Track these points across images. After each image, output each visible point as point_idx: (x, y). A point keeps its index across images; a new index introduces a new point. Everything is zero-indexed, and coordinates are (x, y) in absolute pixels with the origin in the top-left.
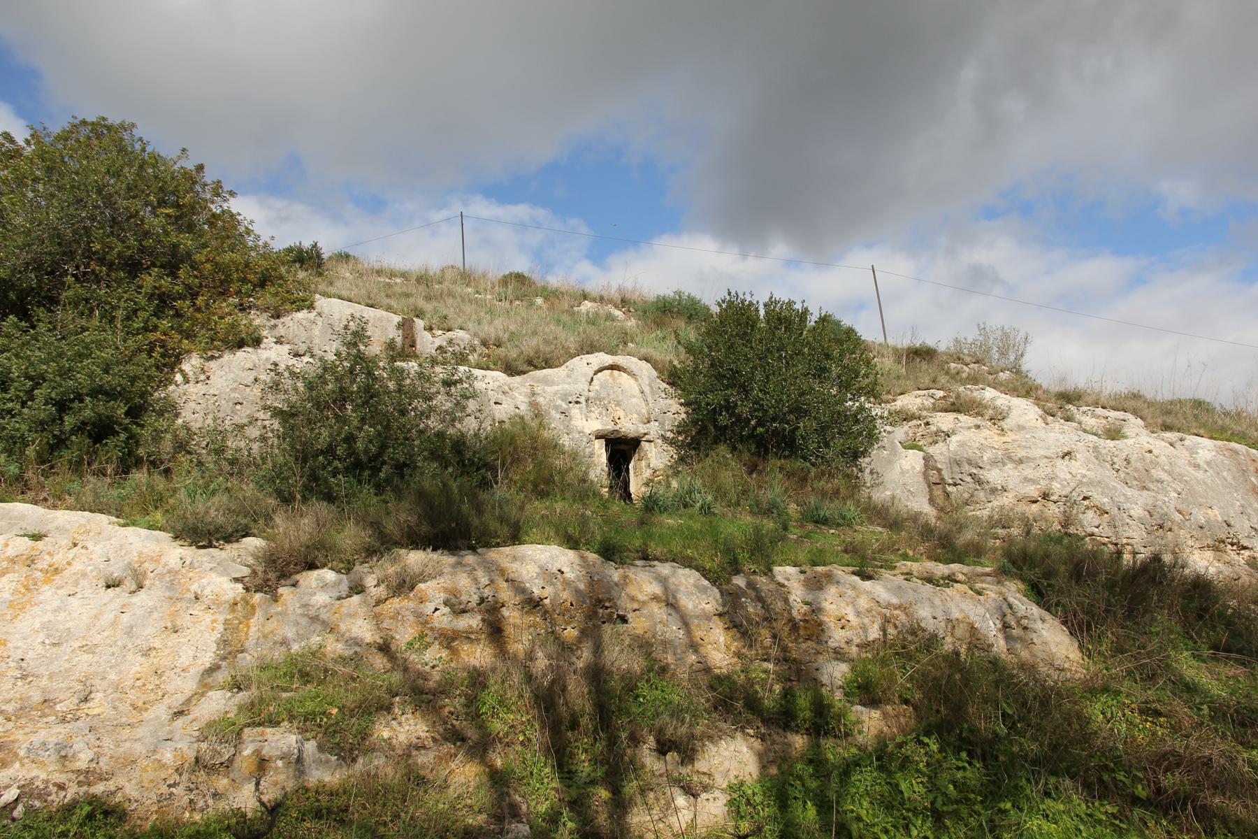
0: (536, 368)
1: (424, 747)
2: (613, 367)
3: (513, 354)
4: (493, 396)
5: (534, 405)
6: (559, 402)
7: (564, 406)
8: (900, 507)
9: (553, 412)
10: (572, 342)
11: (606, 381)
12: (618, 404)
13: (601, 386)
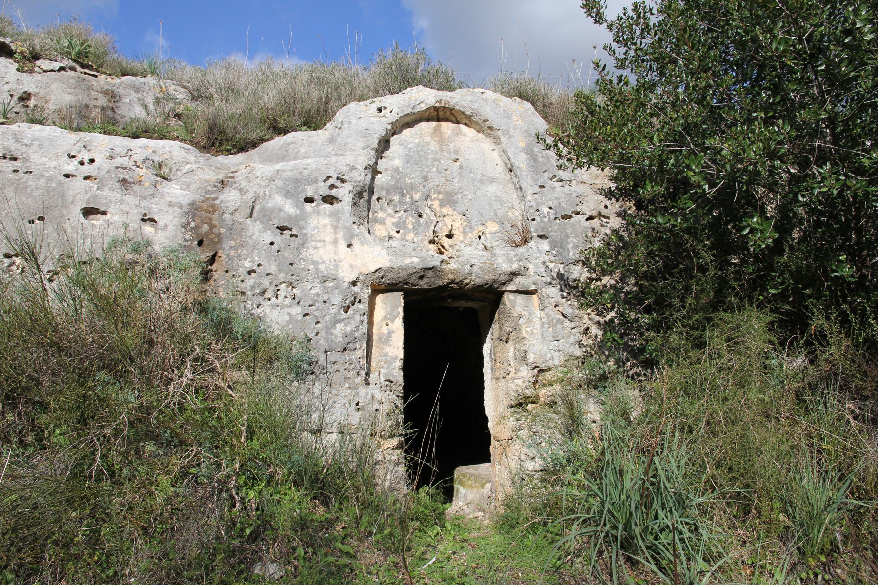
2: (439, 114)
7: (290, 208)
12: (449, 200)
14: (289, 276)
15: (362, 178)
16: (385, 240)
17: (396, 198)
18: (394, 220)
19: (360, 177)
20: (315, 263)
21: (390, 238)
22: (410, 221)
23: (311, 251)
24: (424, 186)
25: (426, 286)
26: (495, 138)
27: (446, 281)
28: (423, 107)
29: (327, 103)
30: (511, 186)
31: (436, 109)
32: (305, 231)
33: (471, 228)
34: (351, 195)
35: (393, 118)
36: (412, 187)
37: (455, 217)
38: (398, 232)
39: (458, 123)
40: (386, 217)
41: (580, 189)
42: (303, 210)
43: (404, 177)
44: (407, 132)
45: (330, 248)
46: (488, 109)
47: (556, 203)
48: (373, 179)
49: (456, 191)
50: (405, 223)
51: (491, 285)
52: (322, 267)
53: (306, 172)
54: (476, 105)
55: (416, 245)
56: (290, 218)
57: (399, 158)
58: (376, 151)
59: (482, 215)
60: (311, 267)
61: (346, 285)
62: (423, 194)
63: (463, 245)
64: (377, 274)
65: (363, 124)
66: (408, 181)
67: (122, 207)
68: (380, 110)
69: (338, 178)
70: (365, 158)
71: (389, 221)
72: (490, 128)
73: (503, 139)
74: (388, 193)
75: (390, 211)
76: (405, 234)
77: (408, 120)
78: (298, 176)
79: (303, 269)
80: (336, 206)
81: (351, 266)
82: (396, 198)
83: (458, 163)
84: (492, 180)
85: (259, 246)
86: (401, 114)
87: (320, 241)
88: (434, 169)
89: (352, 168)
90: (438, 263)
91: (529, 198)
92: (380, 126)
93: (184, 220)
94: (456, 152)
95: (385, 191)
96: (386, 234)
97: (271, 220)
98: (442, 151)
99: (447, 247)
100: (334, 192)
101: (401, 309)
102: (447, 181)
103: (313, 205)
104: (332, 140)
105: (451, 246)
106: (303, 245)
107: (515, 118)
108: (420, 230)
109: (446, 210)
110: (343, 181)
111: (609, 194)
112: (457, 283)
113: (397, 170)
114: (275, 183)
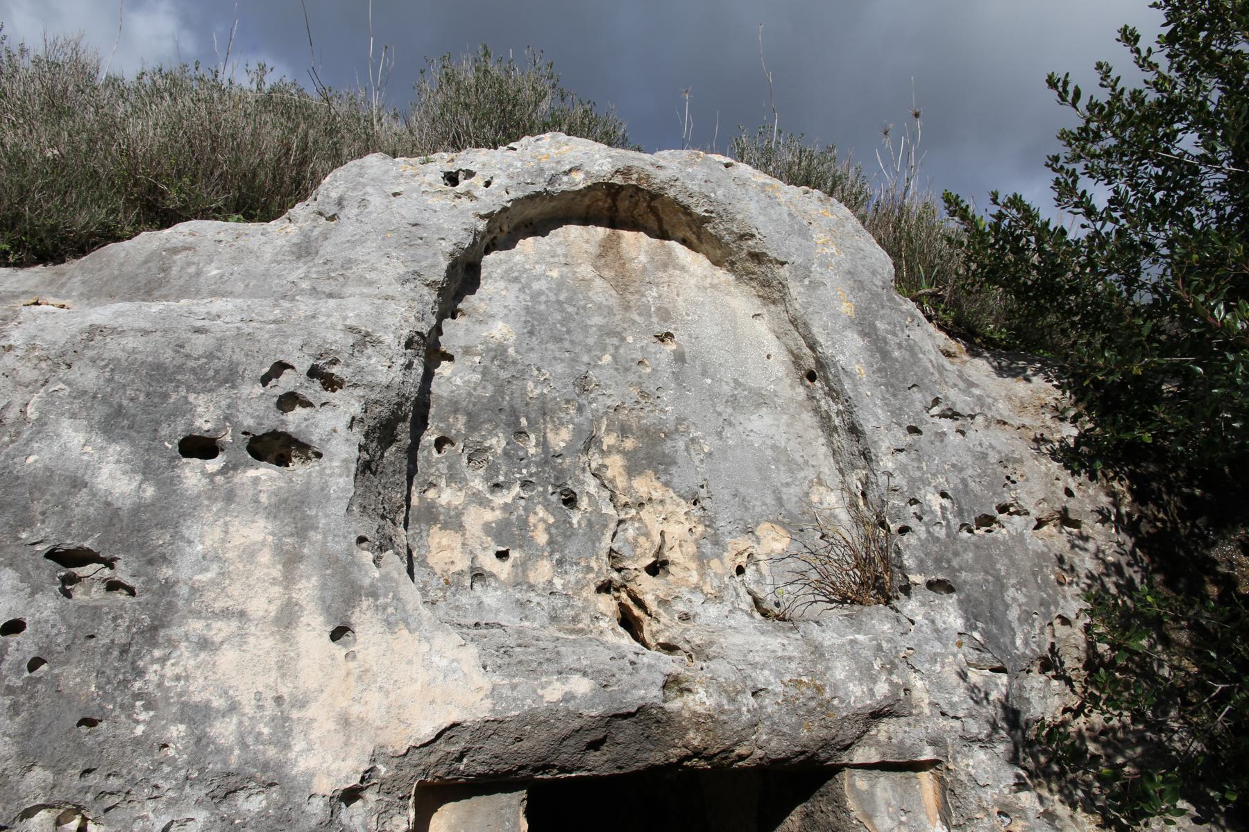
1: (393, 298)
2: (619, 206)
7: (115, 478)
8: (747, 288)
11: (572, 290)
12: (652, 455)
13: (532, 323)
14: (72, 779)
15: (396, 375)
16: (459, 586)
17: (498, 443)
18: (490, 516)
19: (387, 369)
21: (478, 575)
23: (185, 658)
24: (580, 409)
25: (604, 771)
26: (766, 284)
27: (675, 753)
28: (579, 181)
29: (303, 162)
30: (808, 418)
31: (612, 190)
32: (166, 572)
33: (716, 543)
34: (358, 436)
35: (494, 200)
36: (545, 410)
37: (670, 507)
38: (502, 555)
39: (663, 235)
40: (465, 507)
41: (1001, 440)
42: (168, 486)
43: (522, 375)
44: (528, 245)
45: (263, 643)
46: (753, 206)
47: (955, 480)
48: (428, 376)
49: (671, 426)
50: (524, 524)
51: (814, 755)
52: (224, 731)
53: (200, 344)
54: (720, 192)
55: (559, 602)
56: (110, 515)
57: (505, 318)
58: (442, 292)
59: (744, 504)
61: (317, 808)
62: (578, 431)
63: (698, 599)
64: (442, 747)
65: (406, 209)
66: (533, 389)
68: (452, 179)
69: (314, 373)
70: (403, 314)
71: (476, 519)
72: (757, 257)
73: (795, 289)
74: (473, 425)
76: (523, 566)
77: (532, 212)
78: (168, 356)
79: (137, 742)
80: (298, 469)
81: (345, 722)
82: (498, 443)
83: (670, 347)
84: (761, 400)
86: (514, 195)
87: (225, 614)
88: (607, 359)
89: (364, 340)
90: (652, 694)
91: (887, 463)
92: (455, 221)
94: (665, 314)
95: (462, 419)
96: (463, 564)
97: (27, 523)
98: (627, 308)
99: (652, 606)
100: (294, 420)
102: (643, 394)
103: (213, 465)
104: (304, 250)
105: (663, 603)
106: (151, 634)
107: (819, 237)
108: (571, 549)
109: (644, 485)
110: (331, 383)
111: (1070, 457)
112: (709, 758)
113: (498, 353)
114: (74, 374)
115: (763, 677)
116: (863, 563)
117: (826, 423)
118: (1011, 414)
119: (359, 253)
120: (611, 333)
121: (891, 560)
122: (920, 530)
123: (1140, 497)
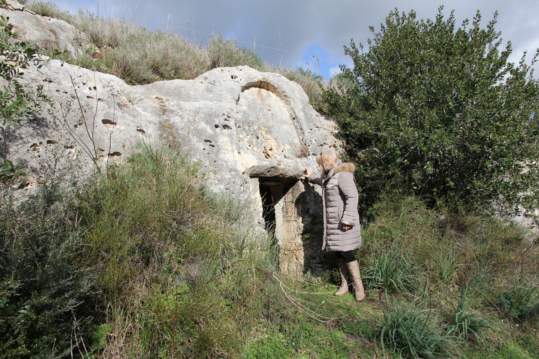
0: (163, 77)
2: (261, 85)
3: (134, 56)
4: (102, 110)
5: (166, 128)
6: (203, 125)
7: (209, 130)
9: (194, 139)
10: (205, 55)
12: (269, 132)
13: (249, 107)
17: (247, 128)
18: (248, 140)
20: (226, 161)
22: (254, 140)
26: (287, 101)
28: (256, 80)
30: (293, 126)
31: (261, 82)
39: (268, 90)
41: (325, 132)
42: (215, 132)
43: (249, 116)
45: (231, 154)
52: (229, 164)
56: (210, 136)
60: (224, 163)
62: (258, 127)
67: (125, 121)
71: (246, 140)
72: (285, 96)
73: (292, 103)
74: (243, 125)
75: (245, 134)
82: (247, 128)
83: (270, 112)
84: (285, 122)
85: (199, 151)
87: (226, 150)
88: (261, 114)
90: (276, 165)
91: (307, 135)
93: (159, 132)
94: (269, 106)
99: (271, 155)
101: (258, 187)
107: (296, 93)
109: (268, 136)
111: (336, 136)
115: (290, 165)
116: (302, 151)
117: (296, 128)
118: (328, 127)
119: (222, 93)
120: (261, 109)
121: (307, 150)
122: (311, 146)
123: (347, 143)
